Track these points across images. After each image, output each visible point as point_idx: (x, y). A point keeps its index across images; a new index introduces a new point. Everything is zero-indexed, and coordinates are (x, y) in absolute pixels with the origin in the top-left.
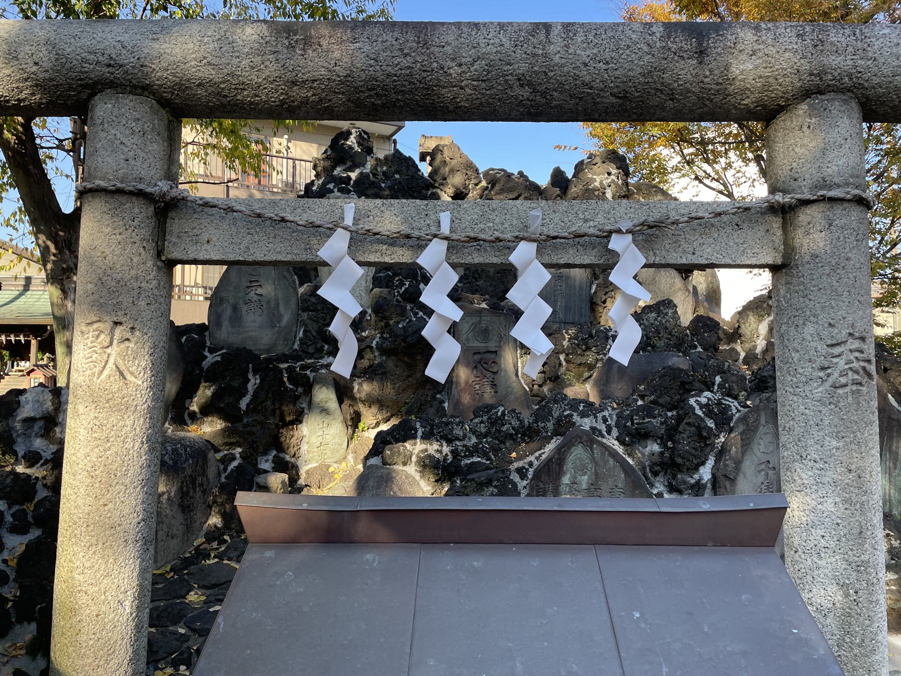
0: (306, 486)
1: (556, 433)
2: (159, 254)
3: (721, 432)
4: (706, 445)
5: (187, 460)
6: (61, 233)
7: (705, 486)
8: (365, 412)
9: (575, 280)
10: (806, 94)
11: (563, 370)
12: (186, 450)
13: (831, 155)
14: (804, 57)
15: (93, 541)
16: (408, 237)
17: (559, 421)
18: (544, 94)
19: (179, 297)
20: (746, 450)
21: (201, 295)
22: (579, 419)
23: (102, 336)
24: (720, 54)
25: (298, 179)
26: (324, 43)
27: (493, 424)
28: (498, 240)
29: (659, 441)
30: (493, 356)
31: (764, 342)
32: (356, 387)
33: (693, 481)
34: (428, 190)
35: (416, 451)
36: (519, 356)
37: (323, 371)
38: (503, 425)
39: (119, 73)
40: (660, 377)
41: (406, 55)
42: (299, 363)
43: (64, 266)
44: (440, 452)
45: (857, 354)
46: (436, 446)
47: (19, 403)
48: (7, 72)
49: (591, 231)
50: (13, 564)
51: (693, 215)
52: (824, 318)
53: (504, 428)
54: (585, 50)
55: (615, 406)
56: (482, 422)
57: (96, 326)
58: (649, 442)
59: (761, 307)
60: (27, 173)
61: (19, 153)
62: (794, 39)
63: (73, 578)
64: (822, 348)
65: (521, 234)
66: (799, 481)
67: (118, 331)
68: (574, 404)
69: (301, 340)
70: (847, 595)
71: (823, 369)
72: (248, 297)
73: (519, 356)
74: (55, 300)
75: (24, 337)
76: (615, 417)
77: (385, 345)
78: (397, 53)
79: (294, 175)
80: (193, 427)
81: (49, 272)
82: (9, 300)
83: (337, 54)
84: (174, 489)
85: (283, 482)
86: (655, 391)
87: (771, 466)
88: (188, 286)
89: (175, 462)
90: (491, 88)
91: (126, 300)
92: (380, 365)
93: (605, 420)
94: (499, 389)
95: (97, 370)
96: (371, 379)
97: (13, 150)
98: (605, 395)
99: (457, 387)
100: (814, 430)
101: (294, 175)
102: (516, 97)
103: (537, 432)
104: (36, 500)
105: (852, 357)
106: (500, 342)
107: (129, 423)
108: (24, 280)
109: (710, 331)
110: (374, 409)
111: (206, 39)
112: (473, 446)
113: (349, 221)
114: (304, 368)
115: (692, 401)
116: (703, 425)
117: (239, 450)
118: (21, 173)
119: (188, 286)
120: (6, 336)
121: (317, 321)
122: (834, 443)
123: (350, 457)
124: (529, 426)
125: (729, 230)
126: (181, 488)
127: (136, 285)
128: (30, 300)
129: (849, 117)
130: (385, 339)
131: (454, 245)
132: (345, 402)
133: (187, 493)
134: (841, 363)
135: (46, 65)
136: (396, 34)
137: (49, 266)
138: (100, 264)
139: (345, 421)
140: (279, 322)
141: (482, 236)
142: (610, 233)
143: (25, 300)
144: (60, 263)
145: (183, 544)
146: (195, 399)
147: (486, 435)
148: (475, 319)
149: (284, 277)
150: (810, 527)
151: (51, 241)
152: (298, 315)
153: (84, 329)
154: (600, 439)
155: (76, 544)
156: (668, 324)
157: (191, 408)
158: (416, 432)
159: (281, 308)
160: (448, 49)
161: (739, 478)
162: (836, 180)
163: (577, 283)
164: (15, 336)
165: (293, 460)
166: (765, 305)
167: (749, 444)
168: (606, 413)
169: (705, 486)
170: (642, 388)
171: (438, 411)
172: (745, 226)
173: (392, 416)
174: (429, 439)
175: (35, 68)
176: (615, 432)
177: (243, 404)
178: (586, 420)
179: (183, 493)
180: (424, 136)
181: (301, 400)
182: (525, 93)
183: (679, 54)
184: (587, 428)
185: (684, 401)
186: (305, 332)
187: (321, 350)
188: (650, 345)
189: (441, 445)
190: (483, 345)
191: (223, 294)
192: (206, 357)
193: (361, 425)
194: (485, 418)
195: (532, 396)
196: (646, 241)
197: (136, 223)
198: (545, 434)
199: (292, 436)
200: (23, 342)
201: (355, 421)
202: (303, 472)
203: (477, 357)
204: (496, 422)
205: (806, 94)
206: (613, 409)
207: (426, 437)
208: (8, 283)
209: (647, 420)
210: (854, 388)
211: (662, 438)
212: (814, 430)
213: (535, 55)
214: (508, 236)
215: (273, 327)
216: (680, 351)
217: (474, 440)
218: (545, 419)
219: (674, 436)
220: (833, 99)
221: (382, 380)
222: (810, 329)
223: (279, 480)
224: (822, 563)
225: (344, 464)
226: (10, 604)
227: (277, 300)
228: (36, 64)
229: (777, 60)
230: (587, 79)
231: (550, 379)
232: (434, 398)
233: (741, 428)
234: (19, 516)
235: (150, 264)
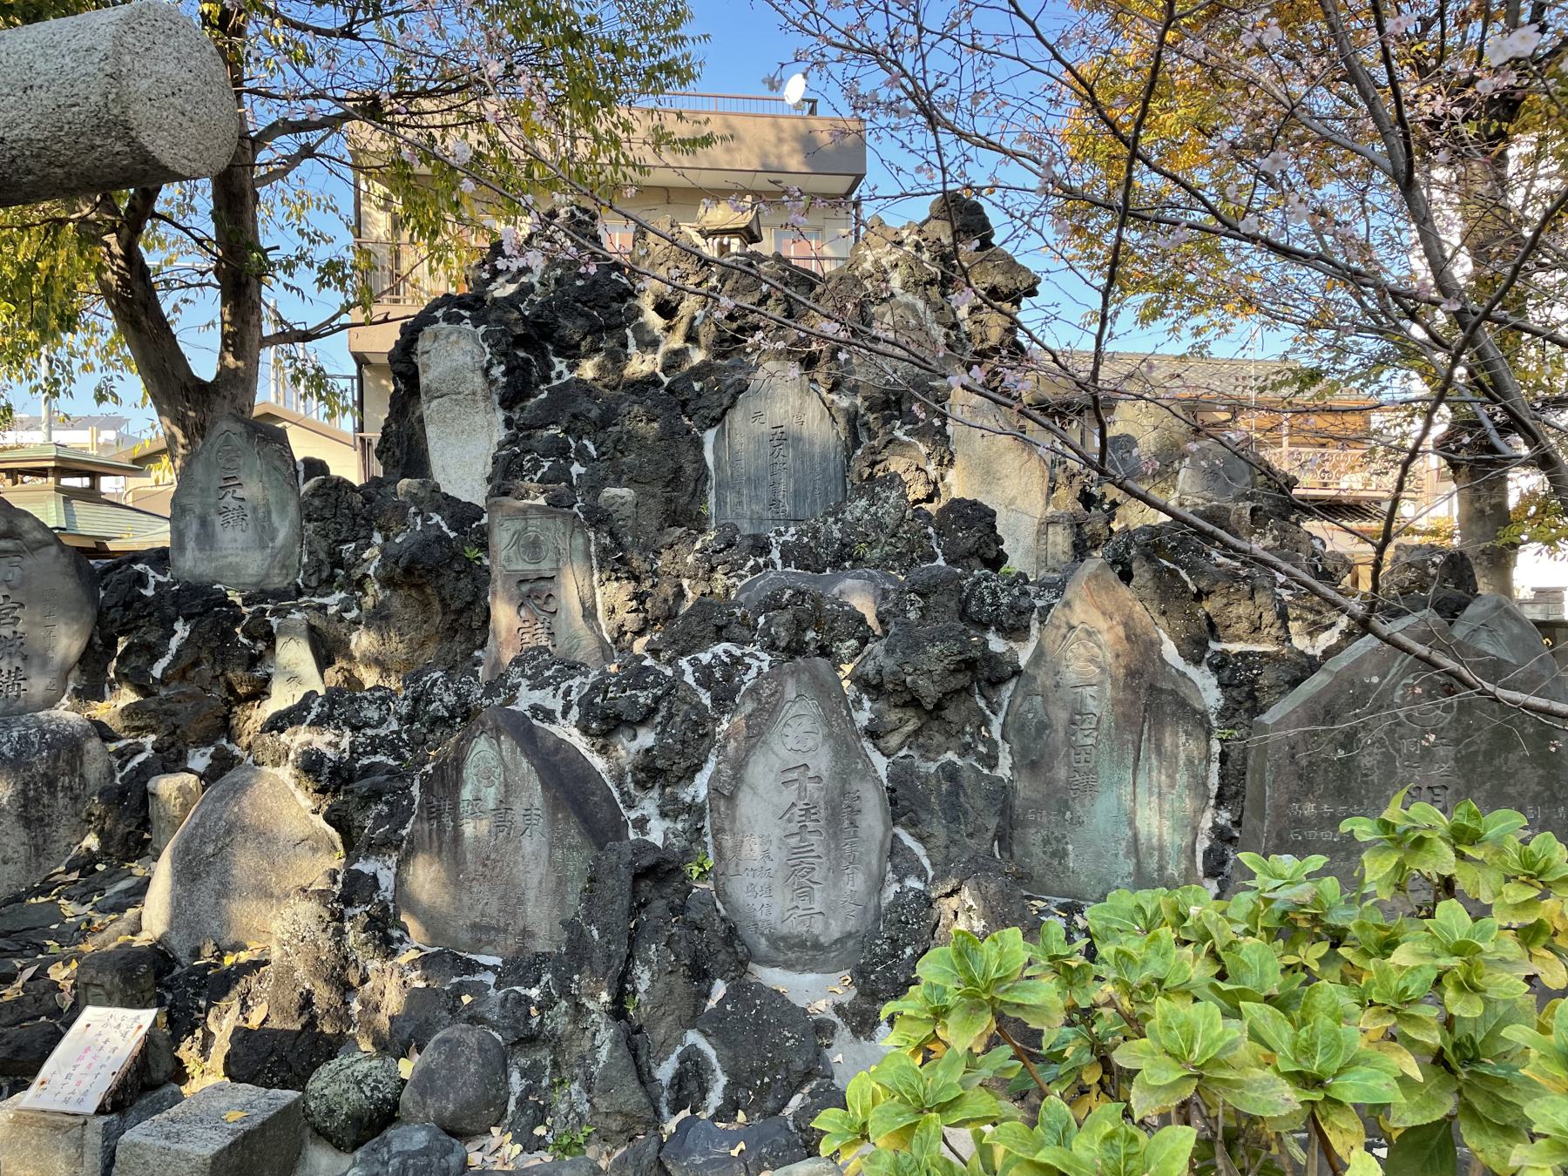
3: (723, 713)
5: (40, 751)
6: (192, 414)
9: (812, 443)
12: (43, 736)
20: (754, 746)
30: (549, 585)
34: (624, 301)
35: (295, 745)
36: (595, 583)
44: (336, 746)
46: (329, 736)
61: (125, 299)
72: (223, 503)
73: (595, 583)
87: (811, 774)
89: (18, 754)
97: (117, 295)
109: (969, 528)
117: (153, 737)
121: (326, 536)
126: (24, 792)
133: (37, 800)
140: (273, 540)
145: (29, 872)
148: (518, 525)
149: (276, 469)
152: (302, 527)
154: (546, 726)
159: (274, 517)
161: (741, 795)
163: (817, 449)
167: (761, 734)
174: (321, 725)
176: (575, 713)
177: (157, 671)
179: (26, 797)
190: (532, 567)
191: (185, 501)
203: (525, 588)
215: (264, 547)
227: (267, 505)
232: (469, 655)
233: (749, 707)
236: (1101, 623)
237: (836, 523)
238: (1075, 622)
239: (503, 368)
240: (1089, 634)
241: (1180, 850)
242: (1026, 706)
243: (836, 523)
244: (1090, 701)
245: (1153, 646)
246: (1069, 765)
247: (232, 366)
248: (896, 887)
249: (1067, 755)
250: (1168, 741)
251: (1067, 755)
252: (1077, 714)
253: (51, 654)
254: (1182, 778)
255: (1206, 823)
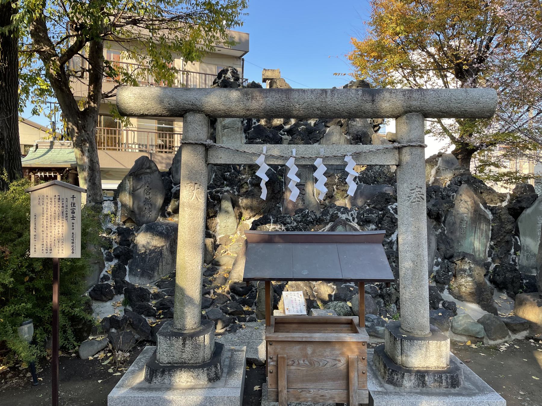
0: (220, 244)
1: (331, 221)
2: (206, 161)
4: (395, 226)
6: (80, 122)
7: (394, 243)
8: (244, 212)
10: (406, 112)
11: (335, 193)
13: (412, 132)
14: (405, 102)
15: (191, 247)
16: (283, 157)
17: (332, 215)
18: (325, 113)
19: (125, 150)
21: (137, 149)
22: (341, 215)
23: (192, 187)
24: (379, 101)
25: (189, 83)
26: (258, 98)
27: (303, 217)
28: (310, 157)
29: (375, 224)
30: (303, 187)
31: (433, 178)
32: (240, 201)
33: (389, 241)
37: (226, 194)
38: (308, 217)
39: (195, 107)
40: (377, 197)
41: (283, 102)
42: (214, 190)
43: (82, 139)
44: (281, 229)
45: (419, 193)
46: (279, 226)
47: (102, 208)
48: (160, 106)
49: (339, 155)
50: (110, 273)
51: (371, 150)
52: (409, 182)
53: (309, 219)
54: (337, 100)
55: (357, 209)
56: (299, 216)
57: (189, 184)
58: (371, 225)
59: (432, 161)
60: (62, 91)
61: (58, 80)
62: (402, 96)
63: (185, 259)
64: (408, 191)
65: (317, 156)
66: (402, 231)
67: (196, 185)
68: (339, 208)
69: (213, 179)
70: (414, 264)
71: (409, 197)
74: (78, 156)
75: (54, 173)
76: (356, 214)
77: (253, 182)
78: (280, 101)
79: (187, 81)
80: (170, 218)
81: (74, 142)
82: (43, 154)
83: (262, 102)
84: (168, 244)
85: (212, 242)
86: (374, 203)
88: (130, 144)
89: (167, 233)
90: (309, 111)
91: (198, 176)
92: (251, 191)
93: (352, 215)
94: (306, 202)
95: (190, 197)
96: (247, 198)
98: (353, 204)
99: (286, 201)
100: (406, 216)
101: (187, 81)
102: (316, 113)
103: (323, 220)
104: (113, 248)
105: (417, 194)
106: (306, 180)
107: (199, 213)
108: (50, 143)
110: (249, 211)
111: (222, 97)
112: (295, 226)
113: (264, 152)
114: (217, 192)
115: (389, 207)
116: (393, 217)
118: (59, 92)
119: (130, 144)
120: (44, 173)
121: (221, 170)
122: (411, 219)
123: (238, 232)
124: (319, 218)
125: (382, 154)
126: (170, 244)
127: (201, 172)
128: (54, 154)
129: (419, 120)
130: (253, 179)
131: (296, 159)
132: (236, 208)
134: (414, 195)
135: (173, 105)
136: (279, 95)
137: (74, 139)
138: (191, 166)
139: (236, 216)
141: (306, 156)
142: (345, 155)
143: (52, 154)
144: (80, 137)
146: (170, 206)
147: (300, 222)
150: (405, 244)
151: (75, 126)
152: (212, 167)
153: (186, 185)
155: (185, 249)
156: (385, 171)
157: (168, 210)
158: (270, 220)
160: (296, 100)
162: (414, 140)
164: (49, 173)
165: (213, 233)
166: (434, 160)
168: (352, 212)
169: (394, 243)
170: (369, 201)
171: (277, 212)
172: (387, 153)
173: (256, 214)
175: (169, 105)
176: (356, 220)
178: (344, 215)
180: (264, 69)
181: (216, 207)
182: (319, 112)
183: (366, 101)
184: (344, 219)
185: (386, 207)
186: (216, 175)
187: (223, 184)
188: (376, 181)
189: (281, 226)
192: (173, 187)
193: (243, 218)
194: (300, 215)
195: (321, 204)
196: (356, 157)
197: (200, 153)
198: (326, 221)
199: (213, 223)
200: (53, 176)
201: (240, 216)
202: (218, 238)
204: (305, 216)
205: (406, 112)
206: (356, 210)
207: (275, 223)
208: (41, 144)
209: (370, 215)
210: (418, 203)
211: (376, 223)
212: (406, 216)
213: (322, 102)
214: (314, 156)
216: (390, 184)
217: (295, 224)
218: (326, 215)
219: (381, 222)
220: (414, 115)
221: (252, 198)
222: (405, 185)
223: (210, 241)
224: (407, 255)
225: (236, 235)
226: (112, 288)
228: (169, 104)
229: (396, 103)
230: (338, 108)
231: (329, 197)
232: (276, 206)
234: (109, 254)
235: (204, 165)
236: (469, 200)
237: (372, 172)
238: (462, 199)
239: (246, 121)
240: (466, 202)
241: (483, 251)
242: (450, 219)
243: (372, 172)
244: (465, 217)
245: (478, 205)
246: (460, 232)
247: (93, 106)
248: (436, 260)
249: (459, 230)
250: (482, 227)
251: (459, 230)
252: (462, 220)
253: (157, 204)
254: (484, 235)
255: (488, 245)
